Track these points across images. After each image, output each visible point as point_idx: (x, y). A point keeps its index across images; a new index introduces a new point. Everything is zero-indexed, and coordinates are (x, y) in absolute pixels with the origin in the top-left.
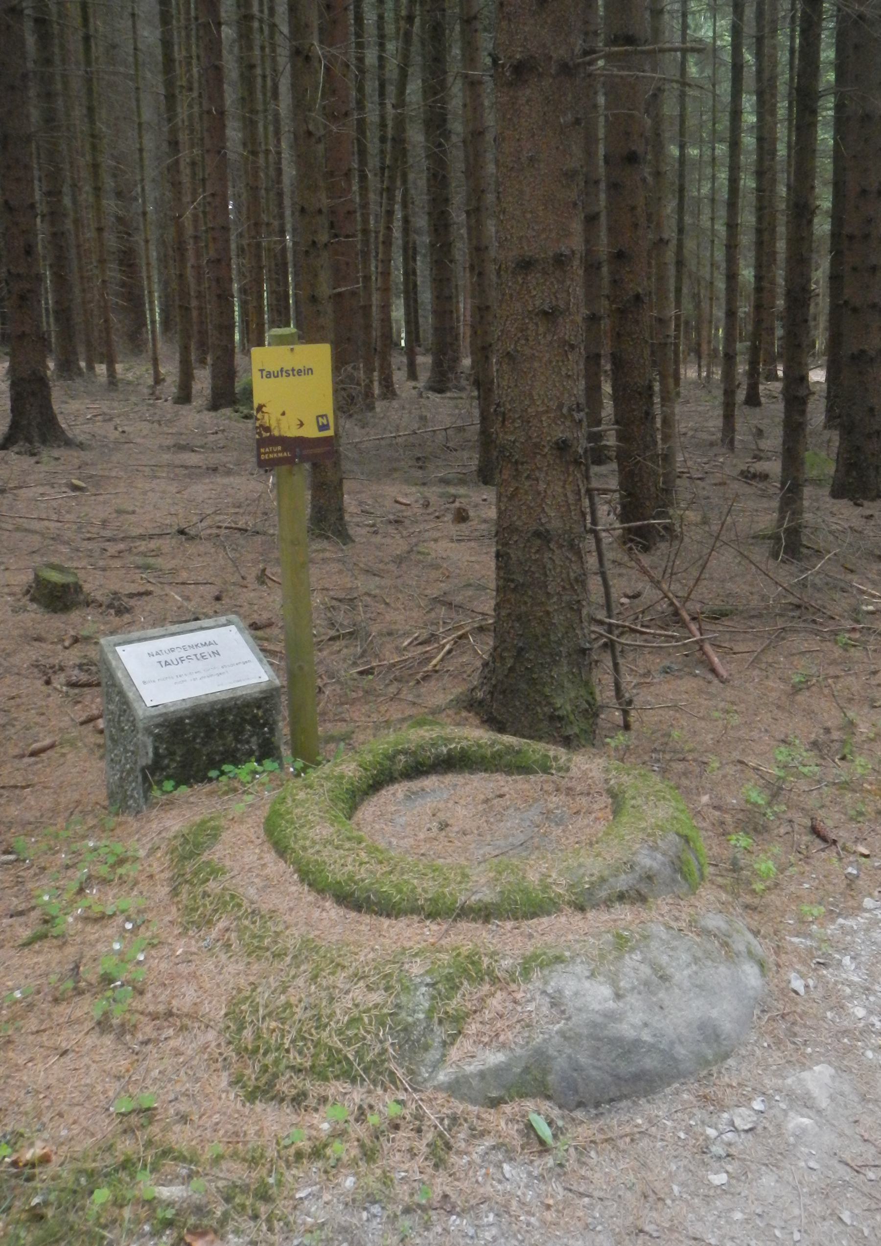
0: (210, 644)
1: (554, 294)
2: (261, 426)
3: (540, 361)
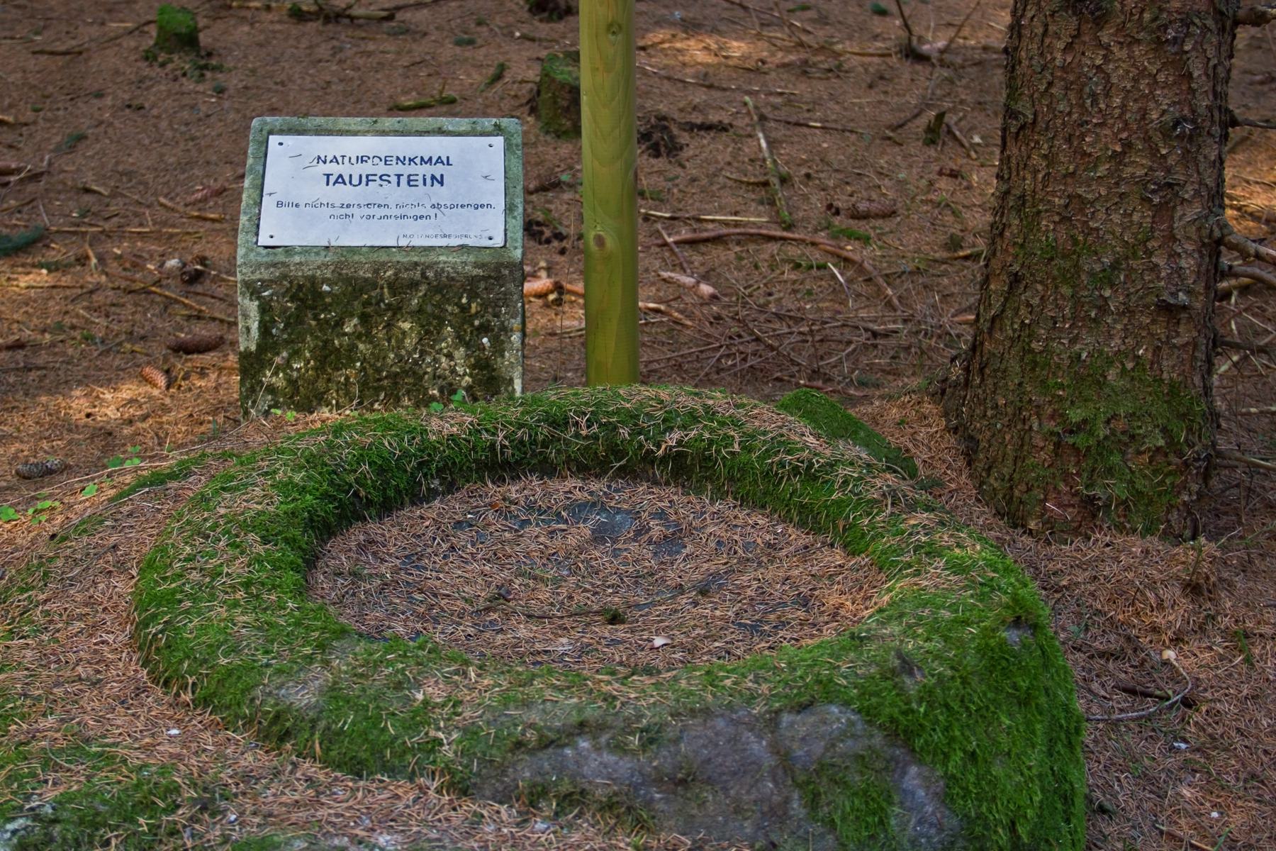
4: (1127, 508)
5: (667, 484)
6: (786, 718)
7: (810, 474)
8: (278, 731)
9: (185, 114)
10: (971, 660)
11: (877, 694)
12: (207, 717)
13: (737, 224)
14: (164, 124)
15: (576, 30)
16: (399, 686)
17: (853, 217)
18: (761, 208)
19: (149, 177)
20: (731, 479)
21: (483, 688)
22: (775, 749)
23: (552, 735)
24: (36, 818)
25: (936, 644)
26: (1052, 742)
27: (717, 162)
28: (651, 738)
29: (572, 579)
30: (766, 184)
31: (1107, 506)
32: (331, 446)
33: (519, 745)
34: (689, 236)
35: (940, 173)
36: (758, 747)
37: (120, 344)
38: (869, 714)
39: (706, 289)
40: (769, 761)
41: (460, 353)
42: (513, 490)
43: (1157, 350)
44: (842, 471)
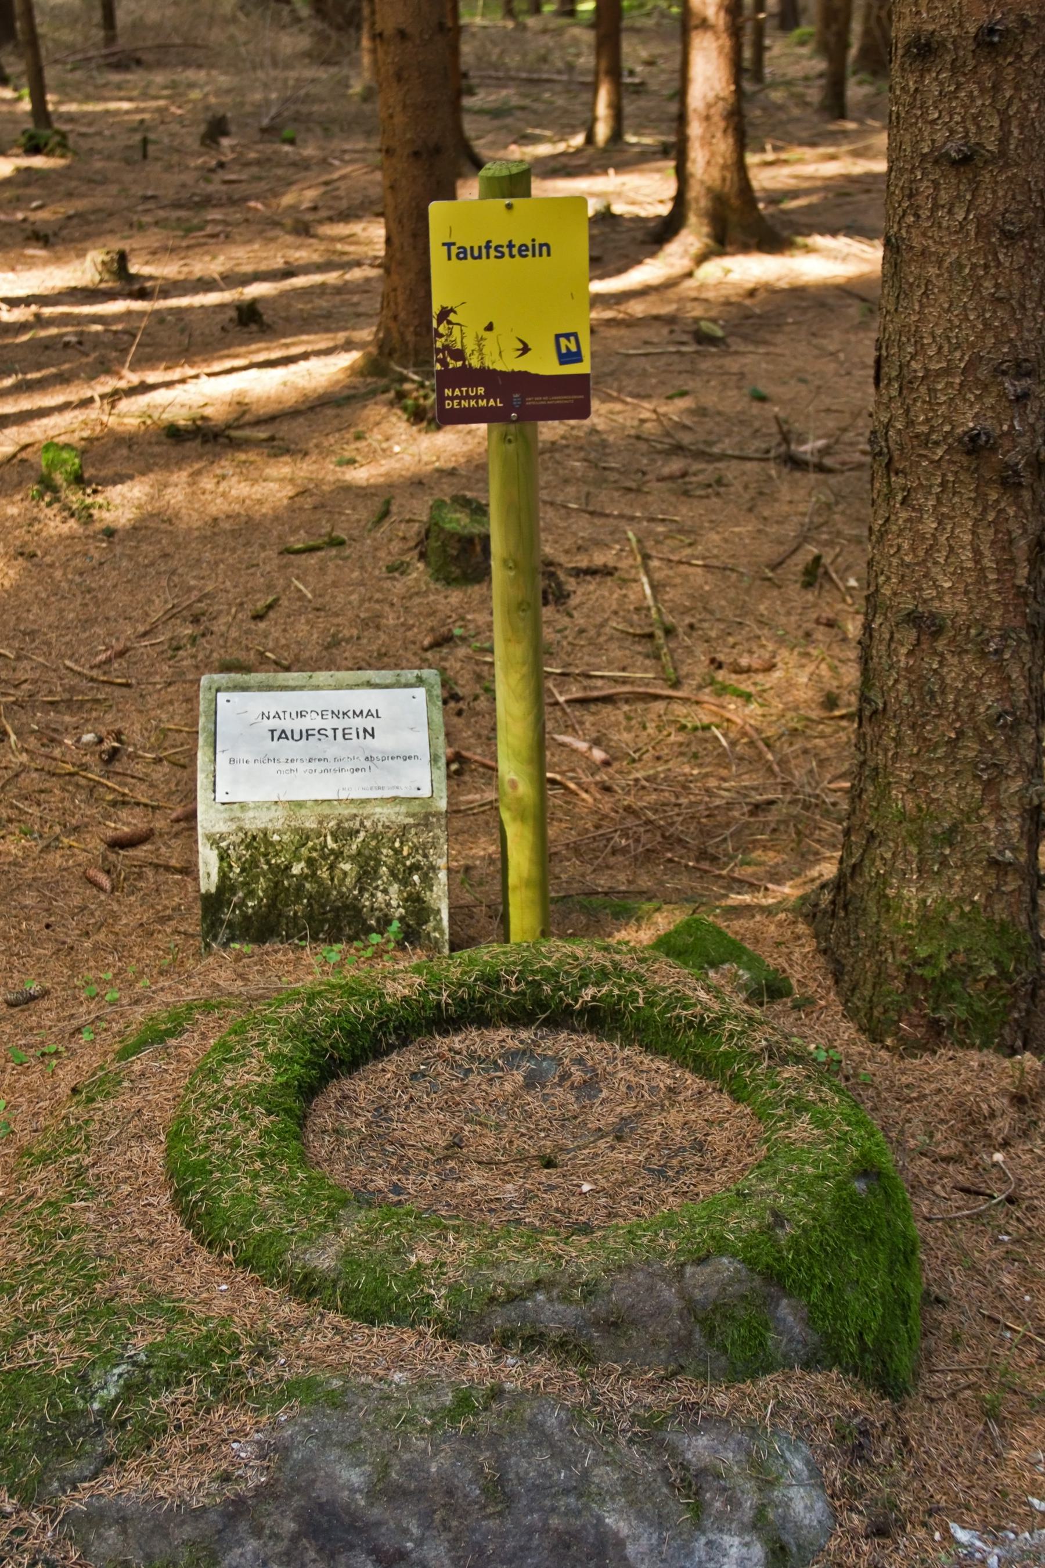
0: (369, 713)
1: (974, 118)
2: (446, 347)
3: (940, 263)
4: (967, 1027)
5: (584, 1032)
6: (689, 1270)
7: (704, 1029)
8: (306, 1287)
9: (78, 562)
10: (827, 1212)
11: (758, 1246)
12: (249, 1276)
13: (624, 681)
14: (58, 574)
15: (486, 600)
16: (397, 1252)
17: (736, 672)
18: (647, 662)
19: (53, 636)
20: (637, 1030)
21: (460, 1249)
22: (682, 1294)
23: (518, 1292)
24: (135, 1364)
25: (802, 1198)
26: (892, 1263)
27: (604, 611)
28: (590, 1290)
29: (511, 1124)
30: (651, 636)
31: (950, 1026)
32: (308, 1015)
33: (492, 1299)
34: (580, 695)
35: (818, 622)
36: (669, 1294)
37: (57, 839)
38: (750, 1263)
39: (598, 755)
40: (677, 1305)
41: (394, 888)
42: (456, 1041)
43: (989, 897)
44: (729, 1025)
